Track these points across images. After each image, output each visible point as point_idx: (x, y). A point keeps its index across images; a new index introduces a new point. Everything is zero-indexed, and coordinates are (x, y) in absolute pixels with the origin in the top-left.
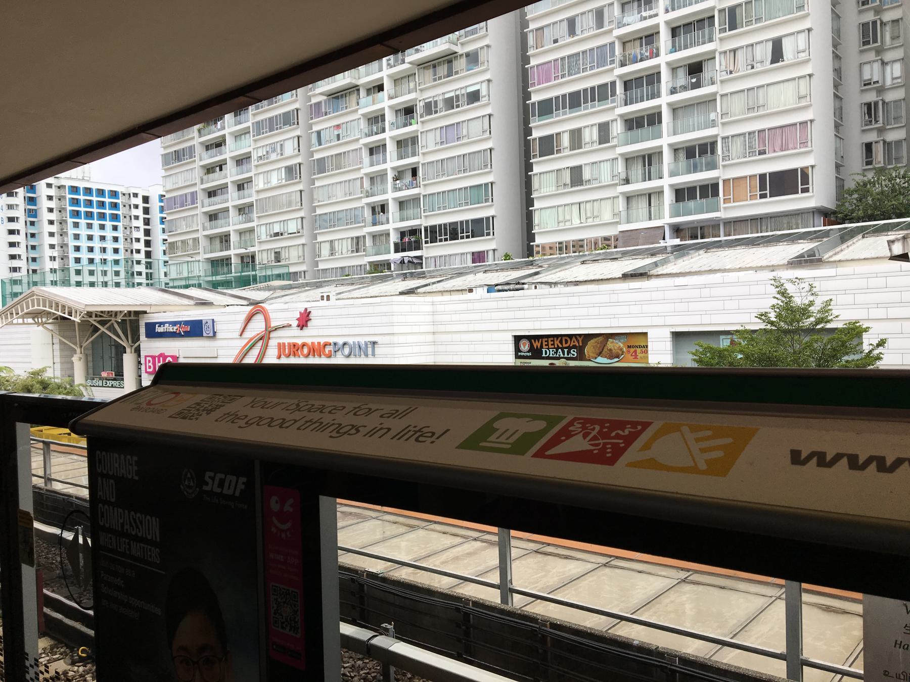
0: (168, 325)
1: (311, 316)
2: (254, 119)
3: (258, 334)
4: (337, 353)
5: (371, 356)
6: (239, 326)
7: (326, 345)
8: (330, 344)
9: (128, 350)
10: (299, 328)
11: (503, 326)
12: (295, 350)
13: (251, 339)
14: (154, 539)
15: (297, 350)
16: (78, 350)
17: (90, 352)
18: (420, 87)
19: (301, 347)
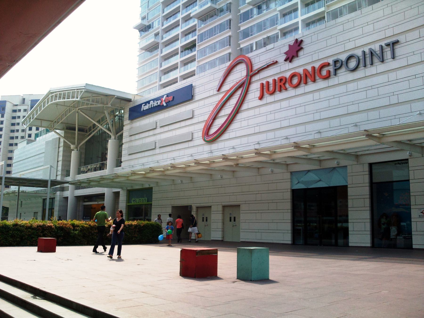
0: (152, 101)
1: (303, 45)
2: (199, 48)
3: (240, 81)
4: (339, 72)
5: (369, 66)
6: (217, 84)
7: (328, 65)
8: (328, 64)
9: (113, 137)
10: (288, 61)
11: (201, 103)
12: (282, 84)
13: (228, 91)
14: (43, 155)
15: (284, 84)
16: (113, 137)
17: (84, 151)
18: (198, 60)
19: (344, 63)
